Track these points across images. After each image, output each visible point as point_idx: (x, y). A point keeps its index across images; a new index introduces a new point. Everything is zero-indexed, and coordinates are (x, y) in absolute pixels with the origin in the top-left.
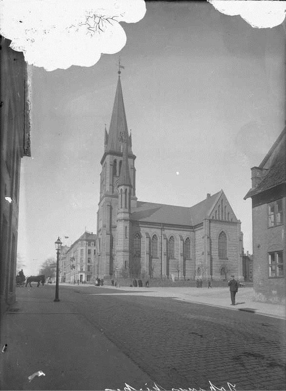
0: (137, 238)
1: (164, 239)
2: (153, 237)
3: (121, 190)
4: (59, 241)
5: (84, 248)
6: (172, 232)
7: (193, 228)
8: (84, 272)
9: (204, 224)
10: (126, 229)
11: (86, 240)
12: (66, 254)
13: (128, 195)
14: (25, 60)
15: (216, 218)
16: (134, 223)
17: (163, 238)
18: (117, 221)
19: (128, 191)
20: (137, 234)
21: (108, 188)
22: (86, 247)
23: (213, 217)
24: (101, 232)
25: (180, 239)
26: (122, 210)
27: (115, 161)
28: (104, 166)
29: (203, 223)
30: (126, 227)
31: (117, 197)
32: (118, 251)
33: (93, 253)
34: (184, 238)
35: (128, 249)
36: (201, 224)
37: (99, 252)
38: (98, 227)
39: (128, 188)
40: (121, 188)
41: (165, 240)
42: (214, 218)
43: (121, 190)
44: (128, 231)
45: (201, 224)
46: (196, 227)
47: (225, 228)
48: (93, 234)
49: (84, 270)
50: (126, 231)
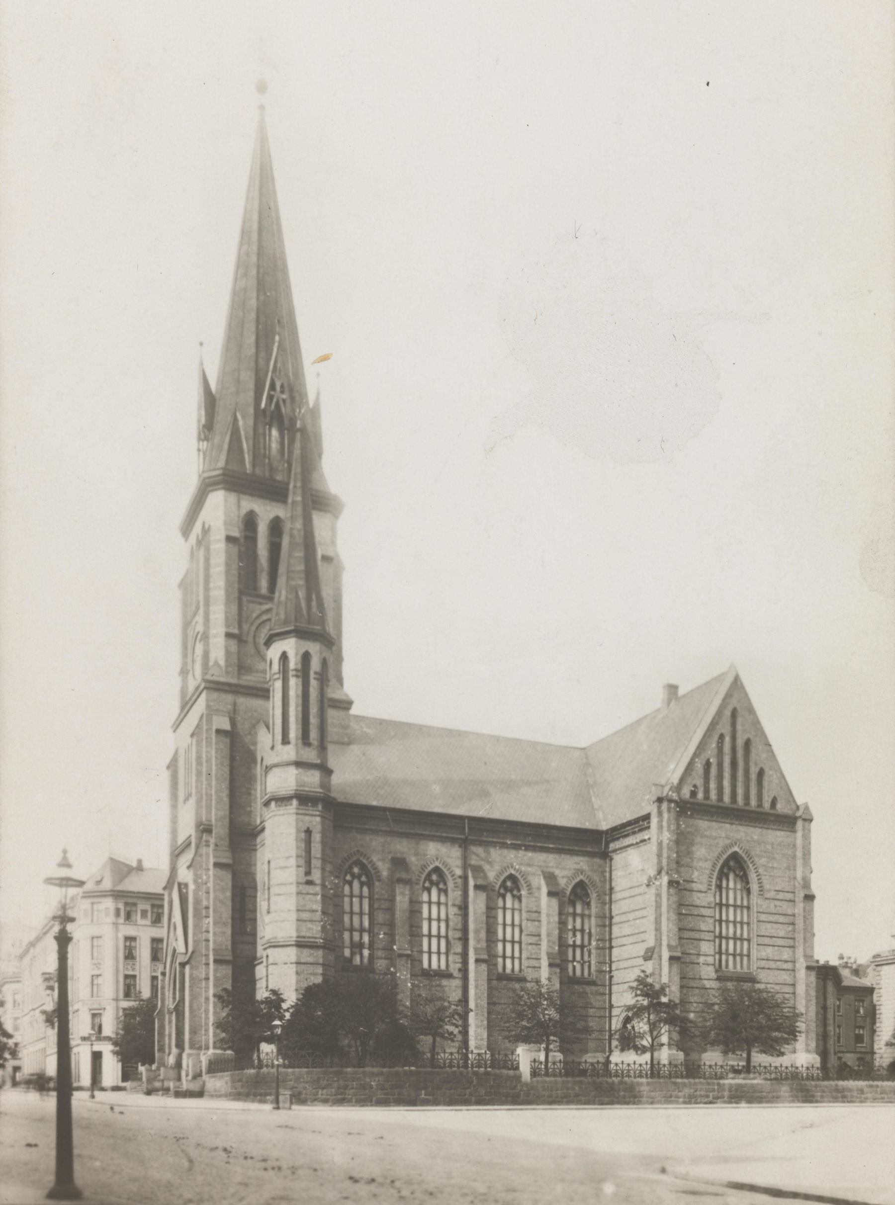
0: (356, 884)
1: (550, 894)
2: (574, 890)
3: (284, 657)
4: (64, 873)
5: (107, 931)
6: (511, 856)
7: (596, 844)
8: (108, 1039)
9: (654, 821)
10: (308, 842)
11: (117, 895)
12: (21, 957)
13: (314, 683)
14: (120, 1064)
15: (707, 791)
16: (346, 825)
17: (471, 883)
18: (267, 804)
19: (315, 665)
20: (357, 863)
21: (219, 649)
22: (115, 924)
23: (693, 794)
24: (187, 857)
25: (544, 890)
26: (289, 752)
27: (250, 522)
28: (199, 542)
29: (647, 817)
30: (308, 832)
31: (264, 693)
32: (275, 945)
33: (144, 952)
34: (562, 882)
35: (314, 931)
36: (636, 821)
37: (181, 948)
38: (174, 832)
39: (314, 648)
40: (274, 653)
41: (483, 896)
42: (700, 796)
43: (284, 657)
44: (317, 849)
45: (641, 823)
46: (619, 831)
47: (743, 836)
48: (146, 865)
49: (109, 1029)
50: (308, 850)
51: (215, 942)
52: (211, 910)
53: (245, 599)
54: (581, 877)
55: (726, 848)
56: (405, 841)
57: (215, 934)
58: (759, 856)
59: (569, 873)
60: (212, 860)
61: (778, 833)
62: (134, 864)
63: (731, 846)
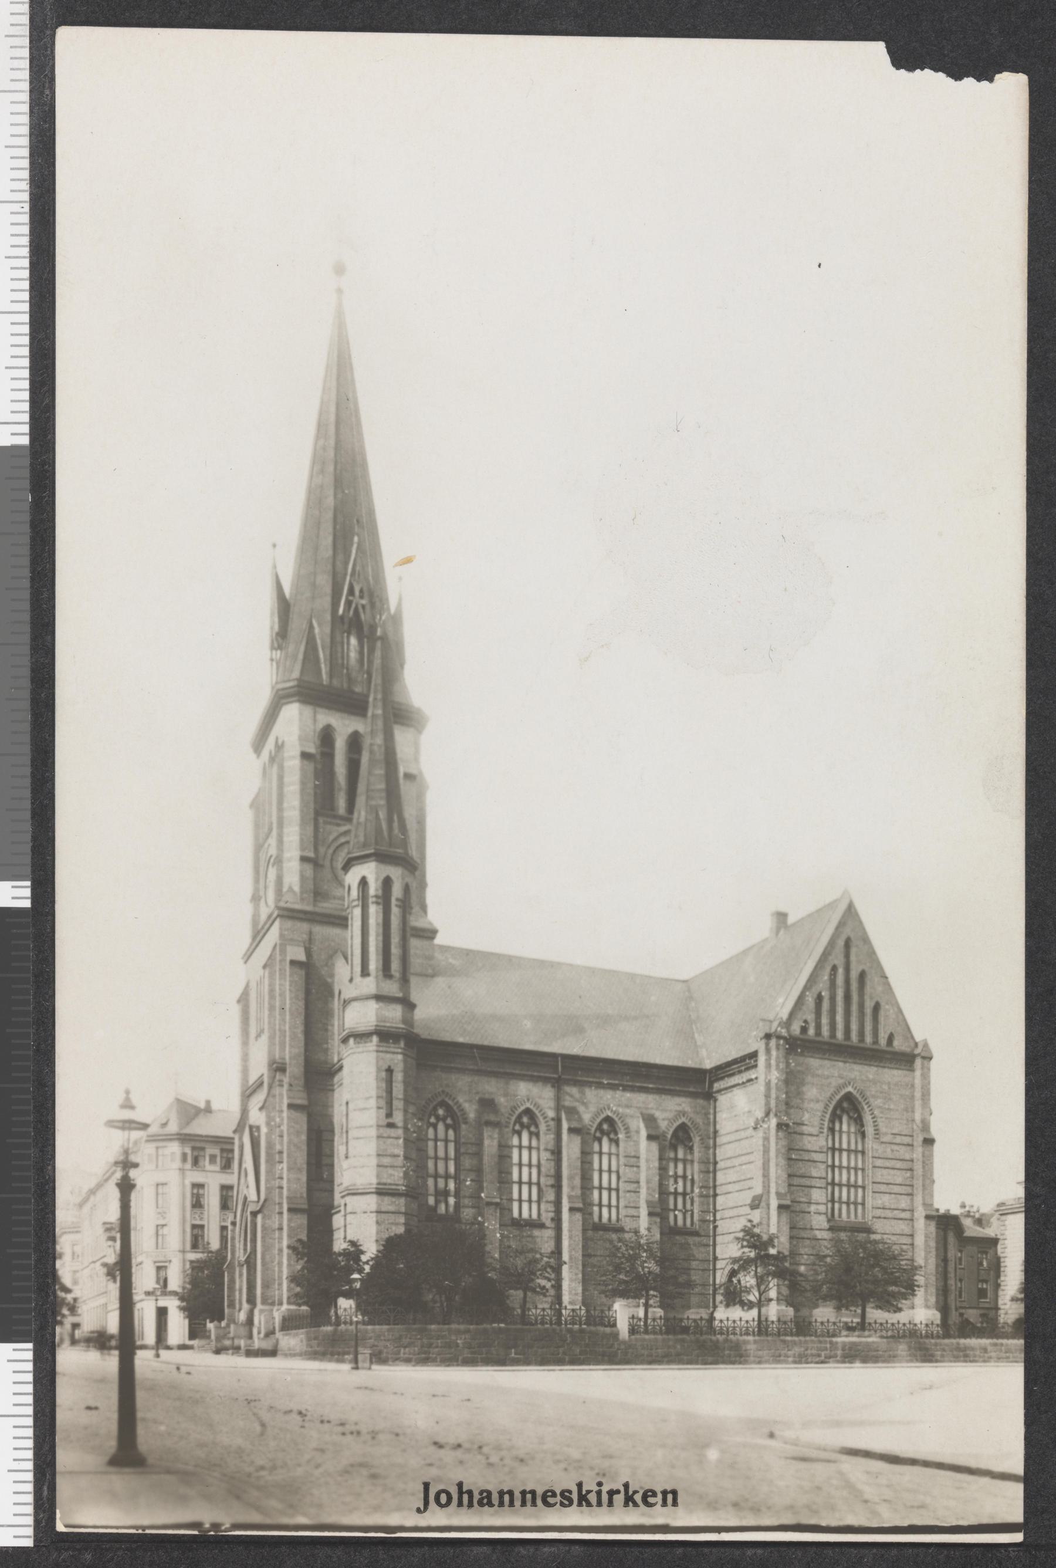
33: (212, 1200)
42: (811, 1032)
48: (214, 1106)
51: (289, 1190)
52: (285, 1155)
53: (321, 820)
54: (683, 1120)
55: (839, 1088)
56: (493, 1081)
57: (289, 1180)
58: (875, 1097)
59: (670, 1115)
60: (286, 1101)
61: (895, 1072)
62: (202, 1105)
63: (844, 1085)
